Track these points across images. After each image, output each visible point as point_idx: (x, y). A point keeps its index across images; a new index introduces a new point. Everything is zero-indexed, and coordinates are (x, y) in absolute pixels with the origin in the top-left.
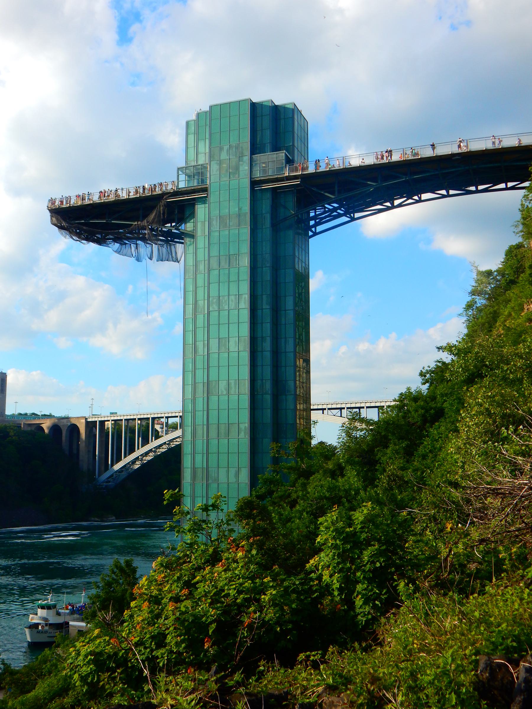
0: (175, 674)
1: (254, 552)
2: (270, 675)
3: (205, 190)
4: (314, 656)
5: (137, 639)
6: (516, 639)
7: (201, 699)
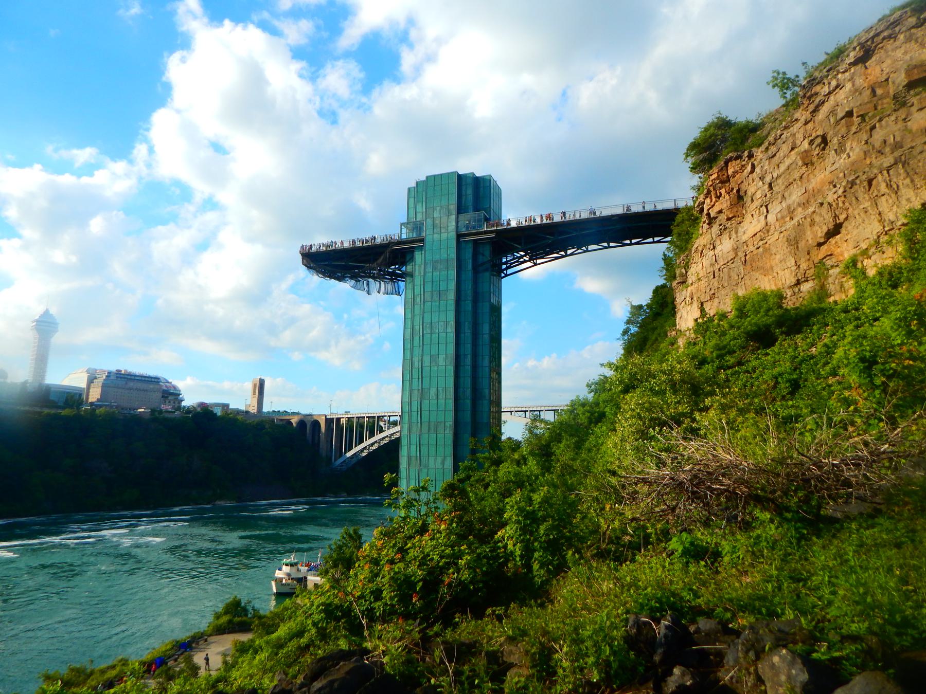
0: (388, 622)
1: (454, 525)
2: (464, 625)
3: (422, 240)
4: (499, 610)
5: (360, 593)
6: (659, 600)
7: (406, 645)
